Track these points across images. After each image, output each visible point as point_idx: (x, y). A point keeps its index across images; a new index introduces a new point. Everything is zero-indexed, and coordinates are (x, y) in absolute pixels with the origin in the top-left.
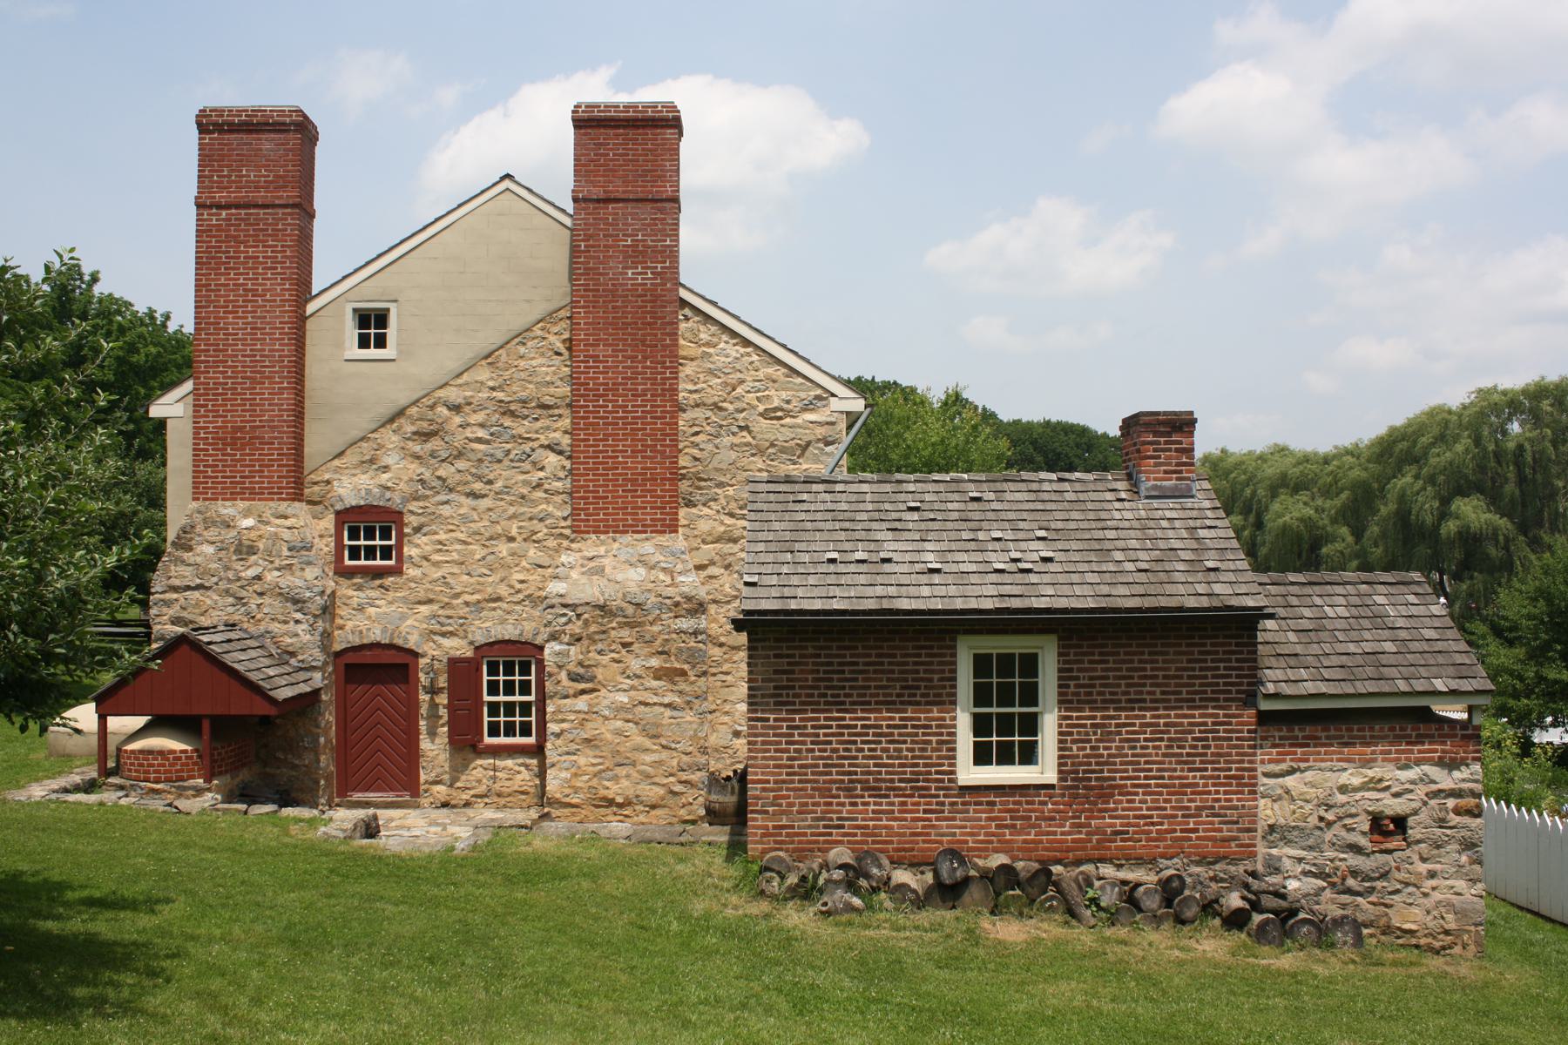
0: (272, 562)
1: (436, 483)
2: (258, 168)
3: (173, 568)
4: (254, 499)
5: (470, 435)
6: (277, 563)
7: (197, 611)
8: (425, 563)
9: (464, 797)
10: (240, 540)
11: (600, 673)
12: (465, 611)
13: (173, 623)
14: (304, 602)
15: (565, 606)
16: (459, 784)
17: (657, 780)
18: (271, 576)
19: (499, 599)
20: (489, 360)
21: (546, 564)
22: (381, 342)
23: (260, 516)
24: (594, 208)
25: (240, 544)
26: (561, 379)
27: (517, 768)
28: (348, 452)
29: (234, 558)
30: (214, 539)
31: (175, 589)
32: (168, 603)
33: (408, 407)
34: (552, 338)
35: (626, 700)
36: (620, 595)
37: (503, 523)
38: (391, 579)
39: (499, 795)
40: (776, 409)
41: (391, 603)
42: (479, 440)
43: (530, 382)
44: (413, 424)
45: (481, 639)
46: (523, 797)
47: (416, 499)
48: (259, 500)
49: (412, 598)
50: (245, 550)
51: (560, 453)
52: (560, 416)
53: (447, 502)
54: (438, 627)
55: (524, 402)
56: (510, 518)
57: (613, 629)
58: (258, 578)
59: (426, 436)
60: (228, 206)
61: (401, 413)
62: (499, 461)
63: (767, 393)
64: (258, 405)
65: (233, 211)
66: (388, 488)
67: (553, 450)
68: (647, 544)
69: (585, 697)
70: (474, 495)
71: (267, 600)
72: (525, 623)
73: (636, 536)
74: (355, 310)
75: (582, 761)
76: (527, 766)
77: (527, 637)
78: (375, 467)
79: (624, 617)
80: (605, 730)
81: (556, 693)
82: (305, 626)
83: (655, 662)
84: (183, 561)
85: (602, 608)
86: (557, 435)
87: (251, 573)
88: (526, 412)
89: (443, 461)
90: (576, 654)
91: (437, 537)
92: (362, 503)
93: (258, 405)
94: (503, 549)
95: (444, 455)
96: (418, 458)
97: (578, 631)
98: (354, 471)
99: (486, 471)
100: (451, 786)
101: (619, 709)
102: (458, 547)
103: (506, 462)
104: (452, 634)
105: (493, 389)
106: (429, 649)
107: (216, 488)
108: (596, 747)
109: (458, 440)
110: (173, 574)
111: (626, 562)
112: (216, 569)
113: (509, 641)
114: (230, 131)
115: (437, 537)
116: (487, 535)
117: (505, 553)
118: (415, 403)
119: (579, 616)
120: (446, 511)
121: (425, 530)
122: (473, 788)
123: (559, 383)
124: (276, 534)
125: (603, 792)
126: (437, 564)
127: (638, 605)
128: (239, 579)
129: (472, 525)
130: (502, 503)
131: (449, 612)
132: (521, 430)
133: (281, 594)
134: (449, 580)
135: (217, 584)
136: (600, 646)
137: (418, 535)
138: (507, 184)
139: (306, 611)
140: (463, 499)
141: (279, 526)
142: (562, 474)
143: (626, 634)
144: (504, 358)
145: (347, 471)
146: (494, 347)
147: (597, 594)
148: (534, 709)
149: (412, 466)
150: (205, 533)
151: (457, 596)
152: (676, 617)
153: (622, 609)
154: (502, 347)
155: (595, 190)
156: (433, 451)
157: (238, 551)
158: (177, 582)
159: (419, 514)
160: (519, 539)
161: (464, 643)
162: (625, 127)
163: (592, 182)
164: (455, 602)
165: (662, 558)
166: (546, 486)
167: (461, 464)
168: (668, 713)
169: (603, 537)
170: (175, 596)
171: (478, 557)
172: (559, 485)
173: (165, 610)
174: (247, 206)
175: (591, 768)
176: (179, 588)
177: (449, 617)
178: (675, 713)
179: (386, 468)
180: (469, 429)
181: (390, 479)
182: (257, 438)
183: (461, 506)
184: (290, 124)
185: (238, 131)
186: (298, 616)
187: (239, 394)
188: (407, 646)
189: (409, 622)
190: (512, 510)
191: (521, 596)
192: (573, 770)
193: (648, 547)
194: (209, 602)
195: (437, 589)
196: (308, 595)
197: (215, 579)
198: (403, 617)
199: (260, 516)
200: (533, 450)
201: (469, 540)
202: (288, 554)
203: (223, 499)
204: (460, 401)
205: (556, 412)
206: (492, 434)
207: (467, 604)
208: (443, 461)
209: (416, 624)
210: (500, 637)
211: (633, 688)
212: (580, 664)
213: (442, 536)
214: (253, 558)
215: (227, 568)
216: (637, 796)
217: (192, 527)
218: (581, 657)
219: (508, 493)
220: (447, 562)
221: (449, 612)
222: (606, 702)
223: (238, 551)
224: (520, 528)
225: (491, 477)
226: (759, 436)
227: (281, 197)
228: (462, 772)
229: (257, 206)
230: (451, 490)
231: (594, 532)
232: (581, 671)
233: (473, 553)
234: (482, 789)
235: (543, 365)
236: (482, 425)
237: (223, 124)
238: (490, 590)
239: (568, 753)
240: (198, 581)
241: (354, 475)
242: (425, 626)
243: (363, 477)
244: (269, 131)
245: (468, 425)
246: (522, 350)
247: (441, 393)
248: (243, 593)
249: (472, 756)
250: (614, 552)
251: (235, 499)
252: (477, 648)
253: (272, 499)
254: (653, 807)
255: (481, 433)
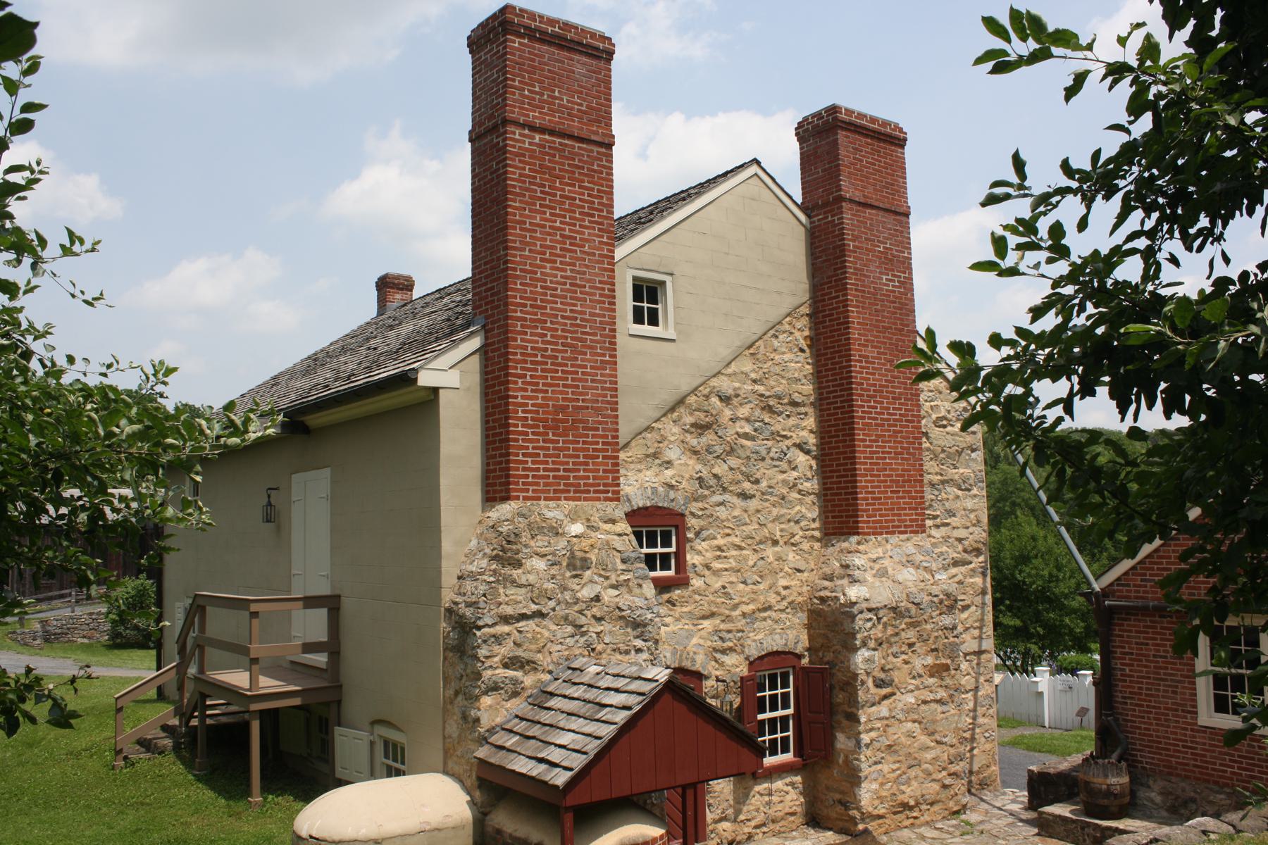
0: (607, 578)
1: (713, 482)
2: (571, 92)
3: (501, 591)
4: (579, 499)
5: (739, 430)
6: (613, 580)
7: (533, 647)
8: (707, 572)
9: (746, 830)
10: (572, 552)
11: (896, 676)
12: (741, 623)
13: (506, 666)
14: (645, 625)
15: (870, 610)
16: (742, 817)
17: (934, 776)
18: (609, 595)
19: (769, 608)
20: (752, 351)
21: (803, 569)
22: (654, 321)
23: (588, 520)
24: (858, 211)
25: (573, 556)
26: (805, 376)
27: (786, 788)
28: (633, 444)
29: (568, 574)
30: (544, 550)
31: (506, 619)
32: (498, 639)
33: (688, 395)
34: (797, 334)
35: (913, 701)
36: (905, 596)
37: (770, 525)
38: (678, 592)
39: (773, 821)
40: (944, 418)
41: (678, 620)
42: (746, 436)
43: (783, 377)
44: (691, 414)
45: (754, 652)
46: (792, 818)
47: (696, 500)
48: (586, 499)
49: (698, 613)
50: (578, 563)
51: (807, 452)
52: (806, 414)
53: (721, 504)
54: (720, 643)
55: (779, 397)
56: (773, 521)
57: (903, 630)
58: (597, 598)
59: (700, 428)
60: (542, 130)
61: (681, 402)
62: (763, 459)
63: (935, 403)
64: (580, 380)
65: (547, 137)
66: (671, 487)
67: (802, 450)
68: (909, 544)
69: (886, 702)
70: (744, 496)
71: (605, 627)
72: (789, 632)
73: (903, 537)
74: (635, 278)
75: (885, 768)
76: (792, 784)
77: (790, 647)
78: (657, 461)
79: (910, 617)
80: (899, 732)
81: (866, 702)
82: (645, 655)
83: (930, 660)
84: (513, 582)
85: (894, 609)
86: (805, 433)
87: (586, 593)
88: (781, 408)
89: (718, 457)
90: (879, 658)
91: (715, 542)
92: (649, 504)
93: (580, 380)
94: (770, 552)
95: (719, 450)
96: (696, 453)
97: (880, 635)
98: (639, 466)
99: (754, 470)
100: (735, 821)
101: (909, 710)
102: (734, 553)
103: (768, 461)
104: (731, 649)
105: (755, 381)
106: (711, 669)
107: (537, 484)
108: (896, 752)
109: (731, 432)
110: (502, 598)
111: (900, 562)
112: (553, 590)
113: (777, 653)
114: (542, 41)
115: (715, 542)
116: (758, 538)
117: (771, 559)
118: (694, 391)
119: (879, 619)
120: (722, 512)
121: (705, 534)
122: (753, 818)
123: (804, 381)
124: (608, 542)
125: (901, 798)
126: (716, 573)
127: (917, 604)
128: (577, 601)
129: (744, 528)
130: (767, 504)
131: (728, 626)
132: (778, 427)
133: (622, 618)
134: (729, 590)
135: (554, 610)
136: (895, 649)
137: (698, 541)
138: (754, 169)
139: (647, 636)
140: (735, 500)
141: (609, 533)
142: (809, 475)
143: (911, 635)
144: (762, 350)
145: (632, 466)
146: (756, 337)
147: (890, 596)
148: (791, 722)
149: (691, 462)
150: (532, 543)
151: (735, 607)
152: (941, 614)
153: (908, 610)
154: (760, 338)
155: (857, 193)
156: (709, 446)
157: (571, 566)
158: (509, 610)
159: (699, 517)
160: (781, 543)
161: (741, 658)
162: (872, 138)
163: (853, 184)
164: (735, 613)
165: (922, 558)
166: (800, 487)
167: (733, 462)
168: (940, 708)
169: (879, 538)
170: (506, 629)
171: (751, 563)
172: (807, 485)
173: (496, 648)
174: (562, 135)
175: (892, 775)
176: (511, 617)
177: (729, 631)
178: (945, 708)
179: (668, 464)
180: (738, 424)
181: (673, 476)
182: (581, 421)
183: (734, 507)
184: (603, 51)
185: (550, 43)
186: (639, 643)
187: (560, 365)
188: (694, 669)
189: (695, 641)
190: (775, 511)
191: (785, 603)
192: (880, 780)
193: (910, 548)
194: (546, 634)
195: (719, 600)
196: (649, 616)
197: (552, 604)
198: (690, 636)
199: (588, 520)
200: (788, 448)
201: (743, 545)
202: (624, 567)
203: (546, 499)
204: (730, 392)
205: (803, 410)
206: (755, 430)
207: (744, 615)
208: (718, 457)
209: (701, 642)
210: (770, 649)
211: (918, 688)
212: (883, 669)
213: (720, 541)
214: (588, 573)
215: (564, 588)
216: (923, 796)
217: (516, 535)
218: (883, 661)
219: (771, 494)
220: (726, 570)
221: (728, 626)
222: (900, 705)
223: (571, 566)
224: (781, 530)
225: (758, 476)
226: (935, 442)
227: (596, 133)
228: (744, 803)
229: (571, 137)
230: (725, 489)
231: (874, 534)
232: (882, 675)
233: (746, 559)
234: (760, 818)
235: (791, 361)
236: (747, 420)
237: (535, 30)
238: (762, 598)
239: (876, 763)
240: (534, 607)
241: (640, 471)
242: (709, 643)
243: (648, 473)
244: (581, 52)
245: (737, 418)
246: (776, 343)
247: (715, 382)
248: (583, 620)
249: (751, 782)
250: (890, 553)
251: (559, 499)
252: (751, 663)
253: (598, 499)
254: (932, 804)
255: (748, 429)
